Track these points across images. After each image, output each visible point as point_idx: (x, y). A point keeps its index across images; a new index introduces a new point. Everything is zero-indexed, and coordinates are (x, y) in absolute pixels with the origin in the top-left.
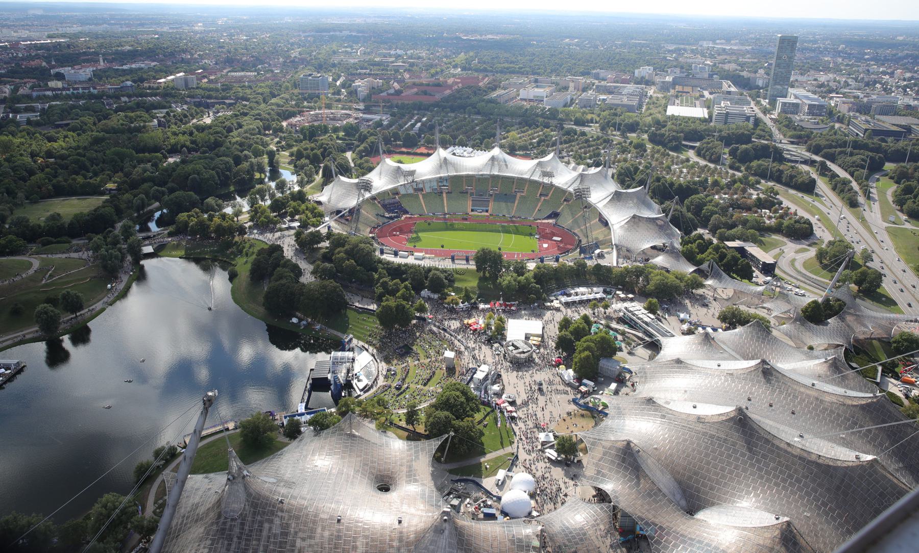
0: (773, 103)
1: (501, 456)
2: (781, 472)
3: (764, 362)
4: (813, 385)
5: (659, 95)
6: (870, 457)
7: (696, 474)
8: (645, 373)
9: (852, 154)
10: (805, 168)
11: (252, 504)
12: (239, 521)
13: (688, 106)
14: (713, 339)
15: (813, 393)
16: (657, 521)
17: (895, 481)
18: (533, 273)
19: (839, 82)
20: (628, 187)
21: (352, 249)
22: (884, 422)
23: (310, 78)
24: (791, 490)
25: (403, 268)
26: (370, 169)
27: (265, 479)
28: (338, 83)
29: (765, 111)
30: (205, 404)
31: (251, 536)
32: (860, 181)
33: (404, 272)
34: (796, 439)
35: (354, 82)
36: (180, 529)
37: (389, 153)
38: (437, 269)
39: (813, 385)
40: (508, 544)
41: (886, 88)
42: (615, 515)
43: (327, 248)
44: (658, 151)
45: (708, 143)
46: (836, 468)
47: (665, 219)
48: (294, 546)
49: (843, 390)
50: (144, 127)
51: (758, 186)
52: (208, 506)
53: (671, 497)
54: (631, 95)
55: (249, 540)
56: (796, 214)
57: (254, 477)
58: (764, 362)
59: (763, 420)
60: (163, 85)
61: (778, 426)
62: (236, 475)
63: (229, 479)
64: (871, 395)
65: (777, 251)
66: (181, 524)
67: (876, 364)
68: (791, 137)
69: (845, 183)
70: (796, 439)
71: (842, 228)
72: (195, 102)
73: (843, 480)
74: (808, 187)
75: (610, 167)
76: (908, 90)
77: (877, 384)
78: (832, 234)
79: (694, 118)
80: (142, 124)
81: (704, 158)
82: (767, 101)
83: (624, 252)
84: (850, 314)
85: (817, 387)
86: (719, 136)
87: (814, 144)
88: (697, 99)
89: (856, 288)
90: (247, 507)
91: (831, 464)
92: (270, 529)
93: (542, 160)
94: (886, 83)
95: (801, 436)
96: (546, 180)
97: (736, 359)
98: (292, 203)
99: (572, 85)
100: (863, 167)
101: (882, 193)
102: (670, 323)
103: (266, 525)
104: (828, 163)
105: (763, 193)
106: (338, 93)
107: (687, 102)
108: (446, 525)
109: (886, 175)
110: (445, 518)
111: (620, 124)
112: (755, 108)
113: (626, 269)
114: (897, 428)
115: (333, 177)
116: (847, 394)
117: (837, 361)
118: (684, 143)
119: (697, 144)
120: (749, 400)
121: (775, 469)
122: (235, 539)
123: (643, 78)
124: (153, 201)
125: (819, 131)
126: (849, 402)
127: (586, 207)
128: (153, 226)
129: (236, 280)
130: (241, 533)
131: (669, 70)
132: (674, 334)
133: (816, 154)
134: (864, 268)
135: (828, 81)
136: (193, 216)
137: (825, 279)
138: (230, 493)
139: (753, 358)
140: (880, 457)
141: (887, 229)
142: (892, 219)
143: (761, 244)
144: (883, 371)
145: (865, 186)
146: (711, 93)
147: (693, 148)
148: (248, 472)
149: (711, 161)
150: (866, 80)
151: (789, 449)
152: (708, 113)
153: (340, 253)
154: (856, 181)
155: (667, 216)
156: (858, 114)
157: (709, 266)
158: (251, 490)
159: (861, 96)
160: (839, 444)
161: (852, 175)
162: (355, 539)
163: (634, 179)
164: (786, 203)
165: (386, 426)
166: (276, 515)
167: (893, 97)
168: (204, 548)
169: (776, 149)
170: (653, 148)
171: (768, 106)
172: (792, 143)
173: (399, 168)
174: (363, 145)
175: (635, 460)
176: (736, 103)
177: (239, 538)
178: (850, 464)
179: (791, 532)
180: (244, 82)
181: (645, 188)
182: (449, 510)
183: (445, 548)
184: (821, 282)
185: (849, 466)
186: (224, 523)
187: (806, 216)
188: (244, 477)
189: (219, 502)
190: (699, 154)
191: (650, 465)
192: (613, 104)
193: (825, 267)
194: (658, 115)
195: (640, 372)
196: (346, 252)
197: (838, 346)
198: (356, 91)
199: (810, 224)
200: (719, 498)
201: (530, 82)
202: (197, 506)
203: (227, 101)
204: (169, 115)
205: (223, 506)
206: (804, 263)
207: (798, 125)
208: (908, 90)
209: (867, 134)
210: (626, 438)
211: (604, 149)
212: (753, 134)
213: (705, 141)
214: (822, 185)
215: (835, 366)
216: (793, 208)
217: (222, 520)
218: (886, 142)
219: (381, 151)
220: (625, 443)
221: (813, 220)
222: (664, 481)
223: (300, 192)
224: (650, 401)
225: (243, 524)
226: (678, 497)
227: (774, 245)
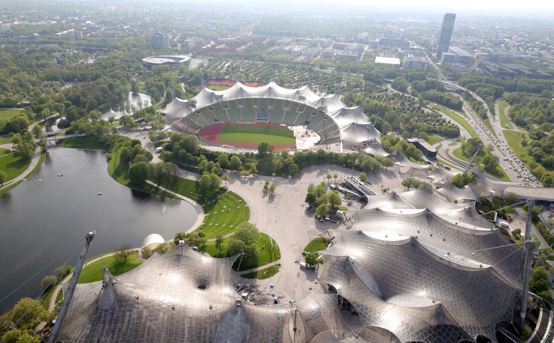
0: (439, 55)
1: (272, 266)
2: (436, 275)
3: (428, 210)
4: (456, 224)
5: (371, 50)
6: (486, 266)
7: (387, 276)
8: (358, 216)
9: (485, 87)
10: (456, 95)
11: (119, 301)
12: (110, 311)
13: (388, 57)
14: (398, 196)
15: (456, 229)
16: (364, 304)
17: (503, 280)
18: (293, 157)
19: (480, 43)
20: (351, 106)
21: (184, 143)
22: (497, 245)
23: (157, 36)
24: (448, 293)
25: (215, 154)
26: (195, 94)
27: (128, 284)
28: (176, 40)
29: (435, 61)
30: (87, 240)
31: (118, 320)
32: (489, 103)
33: (216, 156)
34: (446, 255)
35: (185, 39)
36: (72, 319)
37: (208, 85)
38: (236, 155)
39: (456, 224)
40: (276, 319)
41: (507, 47)
42: (339, 301)
43: (168, 142)
44: (369, 84)
45: (399, 80)
46: (468, 272)
47: (372, 125)
48: (145, 325)
49: (474, 227)
50: (48, 64)
51: (428, 106)
52: (90, 303)
53: (372, 290)
54: (354, 50)
55: (117, 323)
56: (449, 122)
57: (120, 283)
58: (428, 210)
59: (426, 244)
60: (60, 36)
61: (435, 248)
62: (108, 283)
63: (103, 286)
64: (490, 230)
65: (438, 144)
66: (73, 315)
67: (494, 211)
68: (449, 76)
69: (480, 103)
70: (446, 255)
71: (477, 132)
72: (82, 49)
73: (473, 279)
74: (458, 107)
75: (340, 94)
76: (520, 48)
77: (494, 223)
78: (471, 136)
79: (392, 64)
80: (46, 62)
81: (397, 89)
82: (436, 54)
83: (348, 145)
84: (479, 181)
85: (458, 225)
86: (406, 75)
87: (463, 80)
88: (394, 53)
89: (484, 166)
90: (115, 302)
91: (466, 270)
92: (130, 315)
93: (299, 89)
94: (507, 44)
95: (448, 254)
96: (302, 102)
97: (412, 208)
98: (147, 115)
99: (319, 44)
100: (491, 95)
101: (502, 112)
102: (374, 188)
103: (128, 313)
104: (471, 93)
105: (431, 110)
106: (176, 46)
107: (388, 53)
108: (239, 309)
109: (505, 99)
110: (238, 304)
111: (347, 68)
112: (429, 59)
113: (348, 155)
114: (505, 249)
115: (172, 98)
116: (476, 229)
117: (471, 210)
118: (385, 80)
119: (392, 80)
120: (419, 232)
121: (433, 273)
122: (107, 323)
123: (362, 40)
124: (55, 112)
125: (466, 73)
126: (477, 234)
127: (325, 118)
128: (55, 128)
129: (110, 161)
130: (112, 319)
131: (378, 35)
132: (375, 193)
133: (463, 86)
134: (487, 155)
135: (473, 42)
136: (82, 121)
137: (467, 162)
138: (104, 294)
139: (421, 208)
140: (494, 266)
141: (503, 131)
142: (507, 125)
143: (427, 140)
144: (498, 215)
145: (492, 106)
146: (402, 49)
147: (390, 82)
148: (116, 280)
149: (400, 90)
150: (495, 41)
151: (442, 262)
152: (400, 61)
153: (177, 145)
154: (486, 103)
155: (373, 123)
156: (490, 63)
157: (397, 153)
158: (118, 293)
159: (493, 51)
160: (471, 258)
161: (484, 99)
162: (183, 319)
163: (354, 101)
164: (444, 116)
165: (202, 249)
166: (134, 307)
167: (511, 52)
168: (87, 329)
169: (439, 83)
170: (366, 82)
171: (436, 57)
172: (450, 80)
173: (213, 93)
174: (192, 79)
175: (351, 268)
176: (417, 55)
177: (110, 322)
178: (477, 270)
179: (442, 310)
180: (115, 37)
181: (360, 106)
182: (240, 299)
183: (238, 323)
184: (461, 162)
185: (476, 271)
186: (101, 313)
187: (456, 124)
188: (113, 284)
189: (97, 301)
190: (393, 87)
191: (358, 271)
192: (343, 56)
193: (465, 154)
194: (370, 62)
195: (355, 216)
196: (180, 145)
197: (472, 200)
198: (187, 44)
199: (458, 129)
200: (401, 290)
201: (294, 41)
202: (83, 303)
203: (104, 49)
204: (65, 57)
205: (100, 302)
206: (454, 151)
207: (453, 69)
208: (520, 48)
209: (494, 74)
210: (346, 255)
211: (337, 83)
212: (426, 74)
213: (397, 78)
214: (466, 106)
215: (468, 213)
216: (448, 119)
217: (99, 311)
218: (506, 80)
219: (202, 83)
220: (346, 258)
221: (460, 127)
222: (369, 281)
223: (151, 108)
224: (360, 233)
225: (112, 313)
226: (377, 290)
227: (436, 142)
